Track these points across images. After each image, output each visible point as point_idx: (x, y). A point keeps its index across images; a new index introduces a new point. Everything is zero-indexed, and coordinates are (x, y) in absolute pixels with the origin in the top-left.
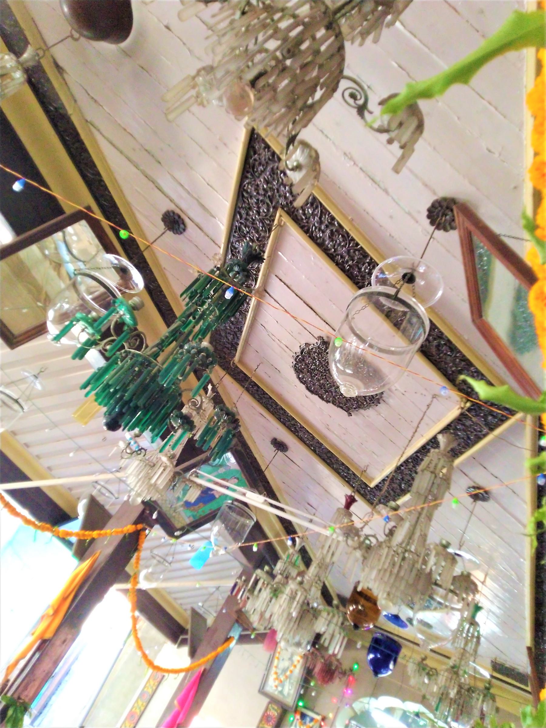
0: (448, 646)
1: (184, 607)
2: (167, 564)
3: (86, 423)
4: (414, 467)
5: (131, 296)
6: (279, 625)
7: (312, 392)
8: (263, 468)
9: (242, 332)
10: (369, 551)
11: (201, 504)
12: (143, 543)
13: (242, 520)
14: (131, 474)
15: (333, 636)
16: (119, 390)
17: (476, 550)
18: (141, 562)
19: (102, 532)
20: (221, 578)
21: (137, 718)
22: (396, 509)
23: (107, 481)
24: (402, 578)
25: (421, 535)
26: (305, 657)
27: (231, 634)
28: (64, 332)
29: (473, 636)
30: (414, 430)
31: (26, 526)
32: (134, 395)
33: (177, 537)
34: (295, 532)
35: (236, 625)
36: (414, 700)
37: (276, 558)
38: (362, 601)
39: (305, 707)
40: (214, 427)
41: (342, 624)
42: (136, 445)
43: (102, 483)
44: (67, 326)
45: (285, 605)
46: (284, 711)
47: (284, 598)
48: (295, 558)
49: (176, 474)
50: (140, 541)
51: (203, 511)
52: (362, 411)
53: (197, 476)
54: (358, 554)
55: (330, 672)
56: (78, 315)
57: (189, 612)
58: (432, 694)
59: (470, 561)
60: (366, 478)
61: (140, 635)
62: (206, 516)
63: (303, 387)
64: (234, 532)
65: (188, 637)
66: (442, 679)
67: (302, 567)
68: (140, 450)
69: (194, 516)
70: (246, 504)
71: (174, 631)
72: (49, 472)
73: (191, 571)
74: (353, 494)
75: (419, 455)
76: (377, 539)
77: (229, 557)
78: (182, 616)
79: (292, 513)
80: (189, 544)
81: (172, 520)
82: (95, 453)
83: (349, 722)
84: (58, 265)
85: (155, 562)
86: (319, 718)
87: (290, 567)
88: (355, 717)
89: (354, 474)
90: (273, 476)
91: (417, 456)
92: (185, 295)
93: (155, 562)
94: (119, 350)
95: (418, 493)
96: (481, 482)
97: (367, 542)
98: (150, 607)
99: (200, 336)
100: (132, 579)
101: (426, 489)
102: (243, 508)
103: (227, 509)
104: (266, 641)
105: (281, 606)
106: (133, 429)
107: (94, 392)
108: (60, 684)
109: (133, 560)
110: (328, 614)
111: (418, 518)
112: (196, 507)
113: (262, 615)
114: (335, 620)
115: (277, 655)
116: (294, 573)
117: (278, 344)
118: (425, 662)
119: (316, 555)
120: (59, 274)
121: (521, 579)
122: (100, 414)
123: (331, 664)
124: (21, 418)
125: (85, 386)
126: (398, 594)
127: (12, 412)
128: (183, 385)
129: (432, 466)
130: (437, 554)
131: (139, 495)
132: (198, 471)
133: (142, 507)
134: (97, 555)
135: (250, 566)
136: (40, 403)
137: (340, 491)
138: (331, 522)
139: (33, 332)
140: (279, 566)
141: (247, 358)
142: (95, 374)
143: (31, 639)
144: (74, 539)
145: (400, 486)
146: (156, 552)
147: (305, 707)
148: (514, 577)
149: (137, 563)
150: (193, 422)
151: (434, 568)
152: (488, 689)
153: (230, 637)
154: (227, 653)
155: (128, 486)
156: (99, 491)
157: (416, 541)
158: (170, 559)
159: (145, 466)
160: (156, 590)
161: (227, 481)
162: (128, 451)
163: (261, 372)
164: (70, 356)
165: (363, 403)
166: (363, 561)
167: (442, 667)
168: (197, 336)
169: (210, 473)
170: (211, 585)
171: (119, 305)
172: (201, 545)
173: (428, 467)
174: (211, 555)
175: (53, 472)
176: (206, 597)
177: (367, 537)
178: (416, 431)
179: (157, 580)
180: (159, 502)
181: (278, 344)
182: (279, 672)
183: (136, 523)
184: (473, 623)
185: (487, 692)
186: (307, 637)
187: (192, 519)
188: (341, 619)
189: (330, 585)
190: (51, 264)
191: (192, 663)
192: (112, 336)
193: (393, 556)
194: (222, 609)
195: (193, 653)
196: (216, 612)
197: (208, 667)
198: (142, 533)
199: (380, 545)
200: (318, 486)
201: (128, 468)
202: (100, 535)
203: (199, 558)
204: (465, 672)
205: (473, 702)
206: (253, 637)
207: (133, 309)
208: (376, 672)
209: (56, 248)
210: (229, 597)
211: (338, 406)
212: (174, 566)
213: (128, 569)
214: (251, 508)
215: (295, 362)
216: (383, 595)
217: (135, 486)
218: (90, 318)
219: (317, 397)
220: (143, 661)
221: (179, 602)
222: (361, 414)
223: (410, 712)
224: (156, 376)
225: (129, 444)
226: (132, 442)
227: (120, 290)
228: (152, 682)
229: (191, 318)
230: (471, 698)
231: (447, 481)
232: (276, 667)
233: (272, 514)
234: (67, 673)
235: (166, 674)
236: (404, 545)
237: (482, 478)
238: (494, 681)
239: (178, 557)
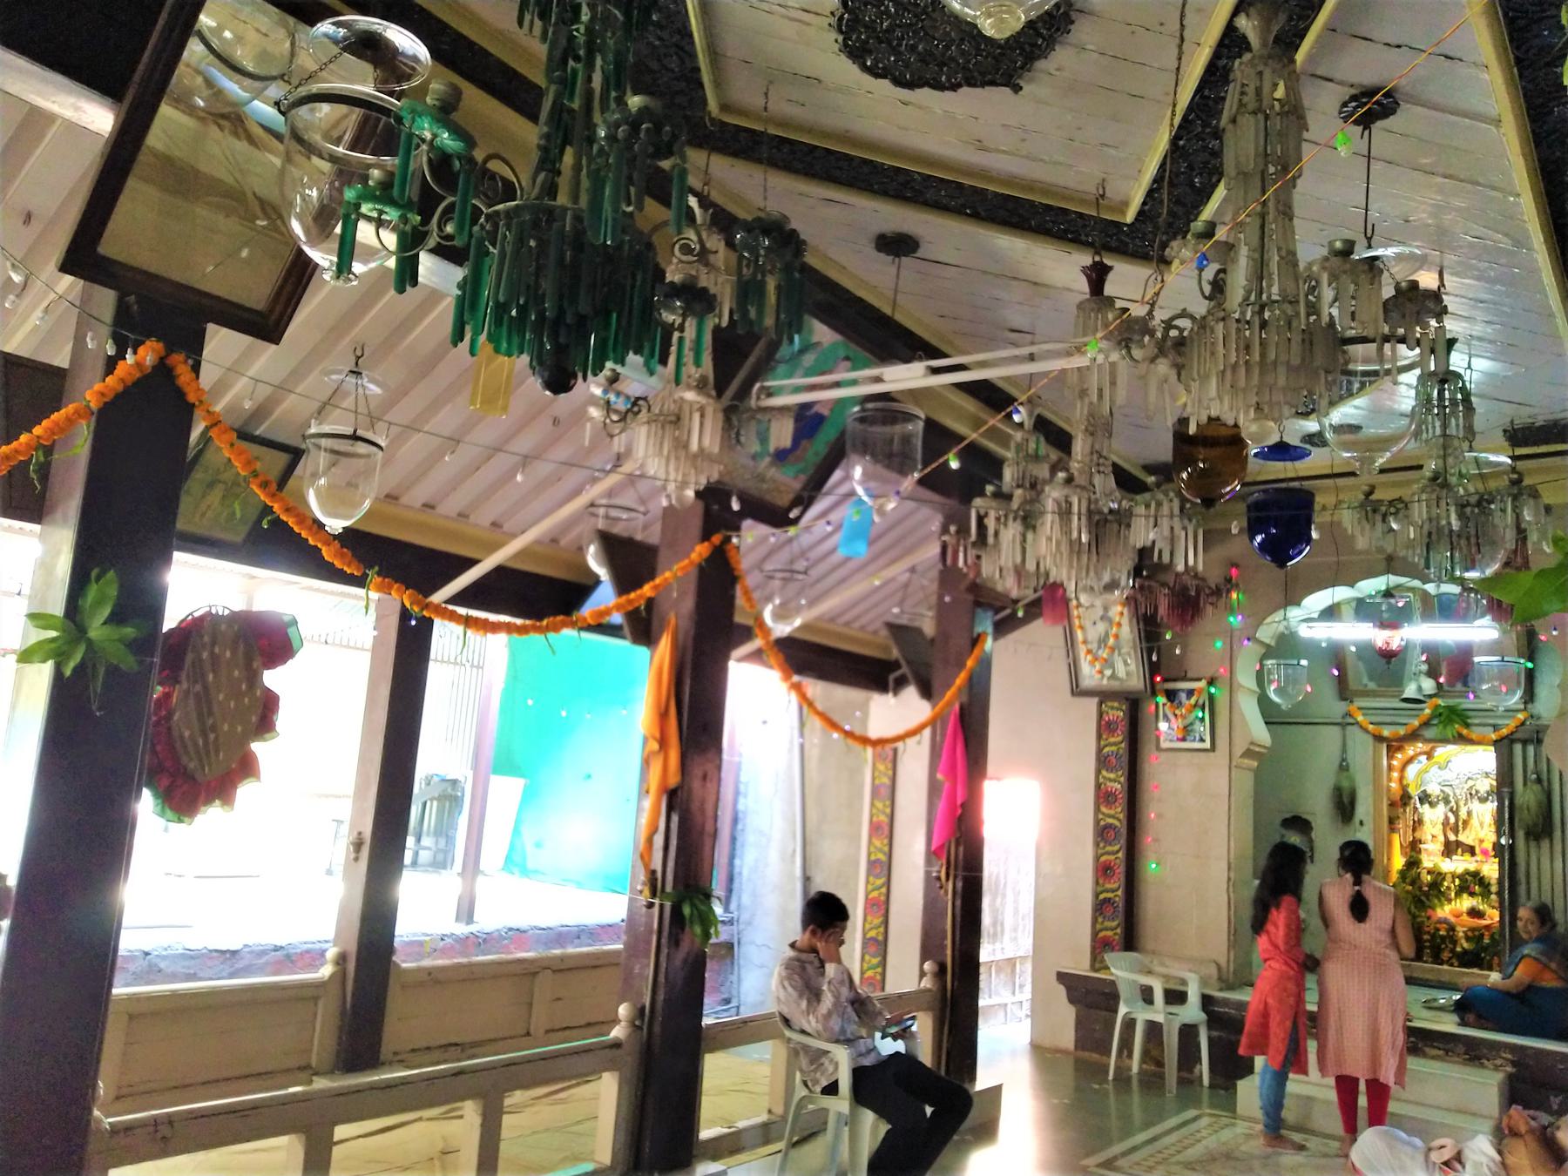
0: (1409, 447)
1: (871, 628)
2: (801, 577)
3: (505, 409)
4: (1205, 125)
5: (422, 90)
6: (1061, 572)
7: (910, 85)
8: (887, 310)
9: (691, 36)
10: (1185, 349)
11: (804, 443)
12: (738, 562)
13: (898, 429)
14: (646, 457)
15: (1172, 540)
16: (526, 302)
17: (1405, 230)
18: (756, 595)
19: (658, 581)
20: (910, 551)
21: (886, 829)
22: (1209, 232)
23: (610, 493)
24: (1275, 363)
25: (1282, 258)
26: (1130, 601)
27: (978, 629)
28: (347, 251)
29: (1454, 402)
30: (1177, 41)
31: (525, 637)
32: (561, 297)
33: (796, 521)
34: (1011, 400)
35: (979, 610)
36: (1371, 574)
37: (994, 466)
38: (1202, 452)
39: (1165, 680)
40: (754, 274)
41: (1182, 509)
42: (621, 399)
43: (604, 501)
44: (342, 237)
45: (1057, 534)
46: (1134, 705)
47: (1049, 522)
48: (1032, 445)
49: (729, 412)
50: (732, 561)
51: (816, 454)
52: (1041, 64)
53: (770, 395)
54: (1163, 367)
55: (1191, 601)
56: (349, 195)
57: (884, 632)
58: (1410, 544)
59: (1399, 257)
60: (1111, 209)
61: (820, 707)
62: (825, 458)
63: (885, 84)
64: (893, 459)
65: (905, 670)
66: (1419, 512)
67: (1054, 455)
68: (634, 404)
69: (802, 471)
70: (885, 397)
71: (875, 675)
72: (499, 533)
73: (851, 566)
74: (1097, 259)
75: (1206, 93)
76: (1192, 317)
77: (911, 505)
78: (880, 646)
79: (983, 365)
80: (823, 521)
81: (768, 497)
82: (562, 452)
83: (1262, 666)
84: (233, 119)
85: (777, 583)
86: (1202, 684)
87: (1030, 467)
88: (1269, 652)
89: (1081, 215)
90: (913, 316)
91: (1203, 97)
92: (527, 17)
93: (777, 583)
94: (474, 221)
95: (1244, 175)
96: (1368, 78)
97: (1174, 333)
98: (806, 658)
99: (613, 94)
100: (757, 631)
101: (1256, 155)
102: (885, 408)
103: (859, 427)
104: (1047, 610)
105: (1049, 539)
106: (602, 368)
107: (483, 337)
108: (733, 839)
109: (740, 601)
110: (1148, 506)
111: (1262, 227)
112: (798, 452)
113: (1019, 571)
114: (1165, 509)
115: (1077, 622)
116: (1043, 471)
117: (783, 16)
118: (1373, 497)
119: (1074, 419)
120: (251, 140)
121: (1521, 242)
122: (519, 370)
123: (1185, 589)
124: (386, 463)
125: (458, 336)
126: (1278, 397)
127: (362, 461)
128: (643, 224)
129: (1250, 99)
130: (1334, 277)
131: (683, 485)
132: (767, 384)
133: (700, 506)
134: (673, 621)
135: (952, 503)
136: (401, 413)
137: (1064, 268)
138: (1075, 336)
139: (289, 288)
140: (1008, 474)
141: (733, 94)
142: (461, 301)
143: (647, 804)
144: (617, 618)
145: (1192, 185)
146: (769, 567)
147: (1165, 680)
148: (1505, 243)
149: (749, 599)
150: (705, 290)
151: (1335, 312)
152: (1516, 483)
153: (979, 635)
154: (986, 664)
155: (654, 478)
156: (607, 517)
157: (1276, 277)
158: (801, 565)
159: (663, 427)
160: (804, 627)
161: (830, 372)
162: (615, 418)
163: (781, 105)
164: (392, 292)
165: (1035, 45)
166: (1179, 375)
167: (1412, 488)
168: (608, 98)
169: (790, 376)
170: (898, 570)
171: (413, 121)
172: (848, 513)
173: (1241, 104)
174: (876, 519)
175: (506, 527)
176: (900, 594)
177: (1168, 325)
178: (1182, 39)
179: (798, 610)
180: (726, 479)
181: (783, 16)
182: (1094, 646)
183: (706, 537)
184: (1446, 377)
185: (1518, 488)
186: (1121, 568)
187: (803, 477)
188: (1176, 504)
189: (1119, 457)
190: (221, 128)
191: (934, 707)
192: (444, 198)
193: (1238, 330)
194: (941, 597)
195: (927, 692)
196: (930, 609)
197: (965, 699)
198: (728, 547)
199: (1202, 324)
200: (1014, 283)
201: (629, 447)
202: (656, 587)
203: (854, 536)
204: (1461, 476)
205: (1497, 519)
206: (1020, 614)
207: (446, 111)
208: (1281, 559)
209: (209, 83)
210: (941, 572)
211: (983, 84)
212: (815, 573)
213: (739, 619)
214: (898, 397)
215: (840, 38)
216: (1247, 413)
217: (667, 473)
218: (374, 189)
219: (926, 91)
220: (850, 741)
221: (857, 625)
222: (1042, 71)
223: (1370, 596)
224: (579, 234)
225: (608, 402)
226: (612, 397)
227: (391, 94)
228: (881, 767)
229: (571, 63)
230: (1491, 513)
231: (1294, 112)
232: (1085, 642)
233: (944, 386)
234: (735, 820)
235: (900, 745)
236: (1253, 298)
237: (1364, 66)
238: (1520, 465)
239: (814, 555)
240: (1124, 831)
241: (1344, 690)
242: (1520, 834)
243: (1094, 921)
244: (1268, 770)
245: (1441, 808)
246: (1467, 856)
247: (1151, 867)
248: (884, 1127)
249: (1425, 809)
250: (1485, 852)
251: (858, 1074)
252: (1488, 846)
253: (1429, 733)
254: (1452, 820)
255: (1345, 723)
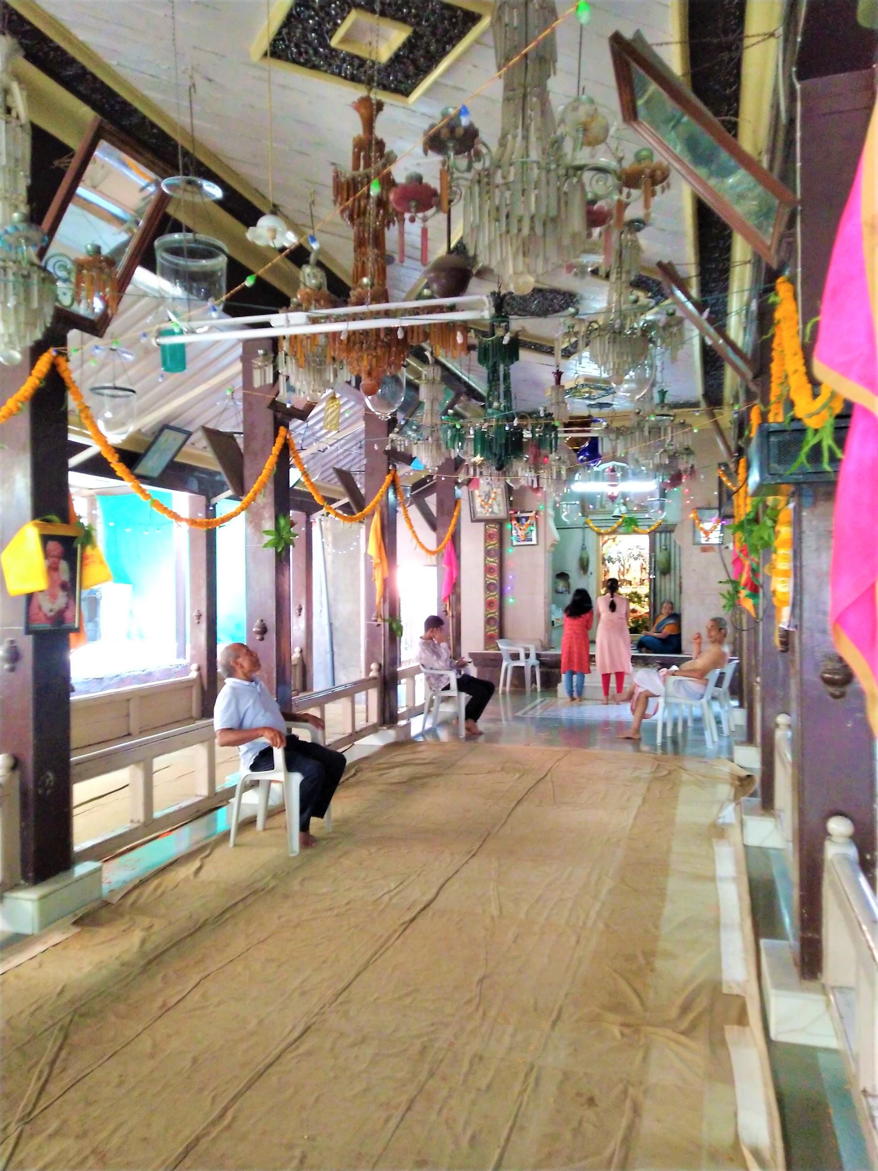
240: (498, 585)
241: (584, 511)
242: (658, 573)
243: (485, 628)
244: (557, 552)
245: (617, 563)
246: (628, 586)
247: (510, 600)
248: (469, 697)
249: (609, 565)
250: (636, 584)
251: (459, 681)
252: (638, 580)
253: (621, 530)
254: (622, 569)
255: (584, 527)
